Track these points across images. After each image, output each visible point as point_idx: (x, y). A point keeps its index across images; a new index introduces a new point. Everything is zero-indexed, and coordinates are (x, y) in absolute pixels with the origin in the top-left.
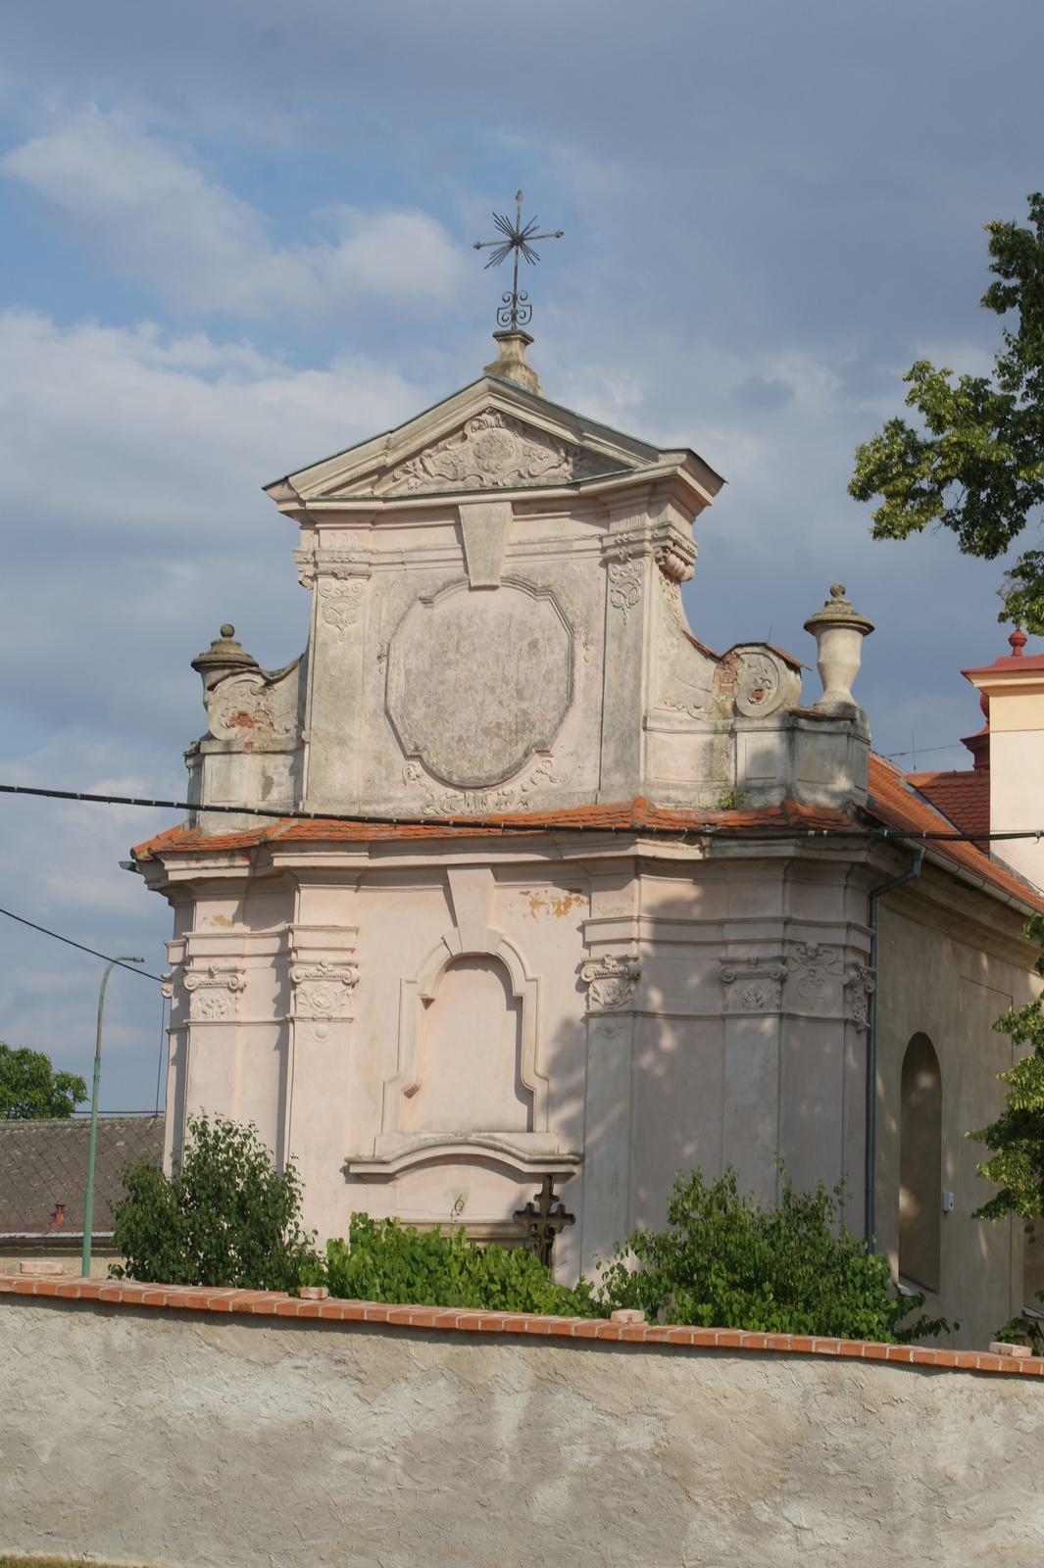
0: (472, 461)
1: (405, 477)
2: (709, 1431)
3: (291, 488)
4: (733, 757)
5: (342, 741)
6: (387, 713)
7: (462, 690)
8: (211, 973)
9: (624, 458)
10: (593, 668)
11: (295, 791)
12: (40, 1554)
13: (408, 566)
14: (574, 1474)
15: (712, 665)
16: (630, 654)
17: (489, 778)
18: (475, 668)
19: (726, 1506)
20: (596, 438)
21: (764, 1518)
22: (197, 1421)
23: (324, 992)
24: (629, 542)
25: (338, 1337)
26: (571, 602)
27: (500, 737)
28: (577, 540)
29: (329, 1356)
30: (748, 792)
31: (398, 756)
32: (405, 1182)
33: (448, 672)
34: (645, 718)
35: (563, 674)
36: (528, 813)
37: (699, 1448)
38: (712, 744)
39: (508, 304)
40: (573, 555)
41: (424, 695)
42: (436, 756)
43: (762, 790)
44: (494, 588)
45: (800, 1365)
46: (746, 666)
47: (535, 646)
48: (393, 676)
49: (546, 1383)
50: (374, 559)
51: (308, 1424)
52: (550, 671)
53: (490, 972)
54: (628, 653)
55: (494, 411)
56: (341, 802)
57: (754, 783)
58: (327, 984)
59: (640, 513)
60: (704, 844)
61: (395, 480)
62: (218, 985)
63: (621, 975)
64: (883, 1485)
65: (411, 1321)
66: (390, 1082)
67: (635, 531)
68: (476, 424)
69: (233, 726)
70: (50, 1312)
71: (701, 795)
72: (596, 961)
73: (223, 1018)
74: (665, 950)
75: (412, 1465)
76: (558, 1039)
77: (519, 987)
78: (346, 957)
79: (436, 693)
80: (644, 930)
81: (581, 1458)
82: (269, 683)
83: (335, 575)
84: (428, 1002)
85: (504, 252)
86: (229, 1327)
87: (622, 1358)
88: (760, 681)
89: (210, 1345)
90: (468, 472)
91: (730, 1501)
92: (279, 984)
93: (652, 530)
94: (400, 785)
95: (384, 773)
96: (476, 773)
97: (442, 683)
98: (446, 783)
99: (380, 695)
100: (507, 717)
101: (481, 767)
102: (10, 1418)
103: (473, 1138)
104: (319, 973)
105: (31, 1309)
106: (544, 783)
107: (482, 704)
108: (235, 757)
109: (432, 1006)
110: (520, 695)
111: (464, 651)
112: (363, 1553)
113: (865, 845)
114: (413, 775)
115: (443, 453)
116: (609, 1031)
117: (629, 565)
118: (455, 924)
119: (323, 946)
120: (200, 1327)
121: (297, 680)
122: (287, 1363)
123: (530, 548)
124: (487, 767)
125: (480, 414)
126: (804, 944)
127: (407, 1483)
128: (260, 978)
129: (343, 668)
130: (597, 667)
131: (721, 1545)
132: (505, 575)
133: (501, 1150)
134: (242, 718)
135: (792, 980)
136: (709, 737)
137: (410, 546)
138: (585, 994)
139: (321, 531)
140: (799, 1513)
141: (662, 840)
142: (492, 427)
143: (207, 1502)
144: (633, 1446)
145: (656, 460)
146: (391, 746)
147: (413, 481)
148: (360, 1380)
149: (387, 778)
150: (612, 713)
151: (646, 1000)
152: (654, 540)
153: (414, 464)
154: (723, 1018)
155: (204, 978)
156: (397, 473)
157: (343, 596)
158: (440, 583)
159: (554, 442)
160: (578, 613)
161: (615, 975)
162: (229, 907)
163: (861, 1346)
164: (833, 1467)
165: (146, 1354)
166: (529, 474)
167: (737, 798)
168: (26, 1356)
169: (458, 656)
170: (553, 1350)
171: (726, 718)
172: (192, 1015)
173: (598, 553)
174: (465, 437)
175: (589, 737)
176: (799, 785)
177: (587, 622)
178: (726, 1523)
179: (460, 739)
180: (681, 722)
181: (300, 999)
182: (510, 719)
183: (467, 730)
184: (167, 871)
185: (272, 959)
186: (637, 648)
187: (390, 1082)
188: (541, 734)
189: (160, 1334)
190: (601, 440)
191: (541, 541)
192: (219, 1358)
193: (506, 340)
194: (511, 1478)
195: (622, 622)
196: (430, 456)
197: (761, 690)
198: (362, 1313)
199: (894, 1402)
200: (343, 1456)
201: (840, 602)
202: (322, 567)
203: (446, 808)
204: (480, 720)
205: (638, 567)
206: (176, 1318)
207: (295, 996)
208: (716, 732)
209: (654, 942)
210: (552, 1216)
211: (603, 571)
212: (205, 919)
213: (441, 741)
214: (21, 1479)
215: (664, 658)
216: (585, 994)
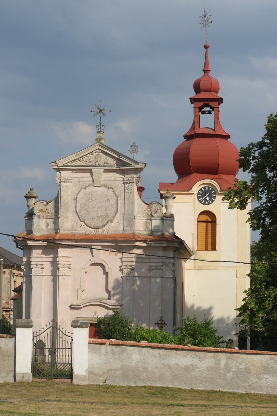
1: (79, 161)
2: (253, 365)
3: (56, 163)
4: (151, 224)
5: (67, 217)
6: (76, 211)
7: (93, 208)
8: (37, 265)
9: (130, 163)
10: (122, 205)
11: (54, 227)
12: (150, 385)
13: (80, 181)
14: (233, 372)
15: (146, 206)
16: (131, 203)
17: (99, 227)
18: (96, 203)
19: (256, 376)
20: (123, 158)
21: (261, 377)
22: (174, 365)
23: (64, 270)
24: (130, 180)
25: (197, 352)
26: (116, 191)
27: (101, 218)
28: (118, 178)
29: (195, 355)
30: (155, 232)
31: (79, 221)
32: (83, 309)
33: (89, 204)
34: (135, 217)
35: (115, 206)
36: (108, 234)
37: (251, 368)
39: (99, 125)
40: (117, 181)
41: (84, 208)
42: (87, 221)
43: (158, 232)
44: (99, 187)
45: (266, 356)
46: (153, 206)
47: (109, 200)
48: (77, 204)
49: (228, 359)
50: (72, 179)
52: (112, 205)
54: (130, 203)
55: (99, 149)
56: (67, 230)
57: (156, 230)
58: (65, 268)
59: (133, 174)
60: (147, 243)
61: (76, 162)
62: (38, 267)
63: (130, 269)
65: (209, 350)
66: (79, 289)
68: (95, 152)
69: (40, 212)
70: (150, 349)
71: (145, 232)
72: (124, 266)
73: (40, 275)
75: (208, 370)
76: (114, 282)
77: (107, 270)
78: (69, 263)
79: (87, 208)
80: (134, 260)
82: (47, 203)
83: (65, 182)
84: (86, 272)
85: (98, 113)
86: (179, 351)
87: (240, 355)
88: (156, 209)
89: (176, 354)
90: (93, 161)
91: (256, 375)
92: (52, 268)
93: (136, 178)
94: (79, 227)
95: (76, 225)
96: (96, 226)
97: (88, 206)
99: (74, 208)
101: (97, 224)
103: (98, 300)
104: (64, 266)
105: (147, 348)
106: (111, 228)
107: (97, 211)
108: (40, 219)
109: (87, 273)
110: (106, 210)
111: (93, 200)
112: (201, 383)
113: (178, 243)
114: (82, 225)
115: (88, 157)
117: (130, 184)
119: (64, 260)
120: (174, 351)
121: (54, 203)
122: (188, 356)
123: (107, 179)
124: (99, 224)
125: (96, 150)
126: (165, 262)
127: (207, 373)
128: (48, 268)
129: (67, 202)
130: (122, 205)
131: (255, 381)
132: (102, 184)
133: (105, 303)
134: (41, 210)
136: (146, 220)
137: (80, 176)
138: (121, 272)
139: (61, 173)
140: (266, 376)
141: (140, 242)
142: (98, 152)
144: (242, 367)
145: (138, 164)
146: (77, 219)
147: (80, 162)
148: (200, 359)
150: (126, 215)
152: (136, 180)
153: (81, 159)
155: (35, 266)
156: (77, 160)
158: (87, 185)
159: (112, 157)
160: (118, 193)
161: (129, 269)
162: (40, 251)
164: (271, 370)
165: (166, 355)
166: (106, 163)
167: (152, 233)
168: (146, 355)
169: (92, 201)
171: (149, 217)
172: (32, 274)
173: (122, 181)
174: (92, 154)
175: (121, 219)
176: (164, 231)
177: (120, 195)
178: (256, 378)
179: (93, 218)
180: (140, 217)
182: (104, 215)
183: (94, 216)
184: (28, 243)
185: (50, 262)
186: (132, 202)
187: (79, 289)
188: (111, 218)
190: (124, 158)
191: (110, 177)
192: (177, 355)
193: (100, 133)
194: (223, 372)
195: (128, 196)
196: (84, 157)
197: (157, 211)
198: (226, 350)
200: (197, 370)
201: (170, 193)
202: (62, 180)
204: (97, 214)
205: (132, 185)
206: (171, 350)
207: (59, 271)
208: (147, 219)
209: (136, 262)
210: (163, 324)
212: (35, 253)
213: (88, 218)
214: (146, 374)
216: (121, 272)
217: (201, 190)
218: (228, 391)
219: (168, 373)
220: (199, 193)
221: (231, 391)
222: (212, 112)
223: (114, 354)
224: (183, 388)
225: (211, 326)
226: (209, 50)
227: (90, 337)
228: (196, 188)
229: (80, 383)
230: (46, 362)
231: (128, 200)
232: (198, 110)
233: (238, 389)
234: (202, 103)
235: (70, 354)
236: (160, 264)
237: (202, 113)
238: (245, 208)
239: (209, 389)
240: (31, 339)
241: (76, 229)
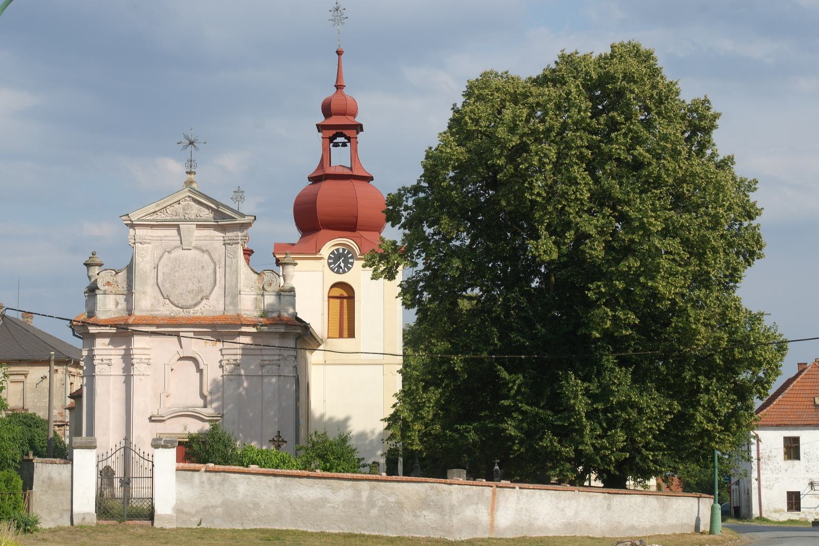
0: (181, 211)
1: (160, 214)
3: (129, 217)
8: (102, 360)
9: (233, 216)
12: (263, 527)
15: (256, 276)
18: (185, 273)
19: (411, 512)
29: (326, 484)
32: (167, 422)
34: (240, 291)
35: (212, 276)
36: (203, 316)
38: (256, 298)
43: (272, 312)
44: (190, 249)
45: (425, 484)
49: (372, 489)
53: (191, 362)
55: (189, 197)
56: (144, 311)
59: (237, 231)
61: (157, 214)
64: (442, 507)
67: (236, 236)
68: (183, 200)
74: (245, 357)
77: (202, 367)
78: (148, 357)
81: (380, 504)
82: (117, 273)
83: (141, 243)
85: (187, 146)
87: (388, 483)
92: (124, 364)
95: (157, 303)
97: (175, 277)
98: (176, 306)
102: (254, 499)
103: (190, 409)
107: (187, 284)
110: (199, 281)
112: (335, 524)
114: (166, 303)
115: (173, 208)
116: (231, 380)
118: (181, 347)
120: (297, 479)
124: (189, 302)
127: (343, 510)
133: (199, 413)
134: (108, 283)
135: (281, 365)
136: (255, 296)
140: (425, 513)
143: (299, 515)
145: (245, 218)
147: (163, 215)
149: (158, 304)
151: (240, 372)
154: (262, 376)
155: (100, 361)
156: (158, 213)
159: (208, 207)
161: (233, 364)
164: (432, 503)
165: (285, 485)
167: (265, 314)
170: (374, 482)
174: (179, 203)
179: (181, 294)
181: (134, 369)
185: (121, 356)
186: (237, 271)
191: (205, 236)
192: (301, 485)
194: (365, 508)
199: (444, 491)
200: (329, 505)
203: (177, 314)
208: (258, 295)
211: (224, 247)
215: (244, 273)
217: (333, 253)
218: (373, 534)
220: (330, 258)
221: (377, 533)
222: (348, 144)
224: (309, 530)
226: (343, 57)
227: (178, 461)
228: (327, 250)
229: (164, 527)
230: (116, 497)
232: (328, 140)
234: (334, 132)
235: (150, 485)
236: (277, 358)
237: (333, 146)
238: (395, 278)
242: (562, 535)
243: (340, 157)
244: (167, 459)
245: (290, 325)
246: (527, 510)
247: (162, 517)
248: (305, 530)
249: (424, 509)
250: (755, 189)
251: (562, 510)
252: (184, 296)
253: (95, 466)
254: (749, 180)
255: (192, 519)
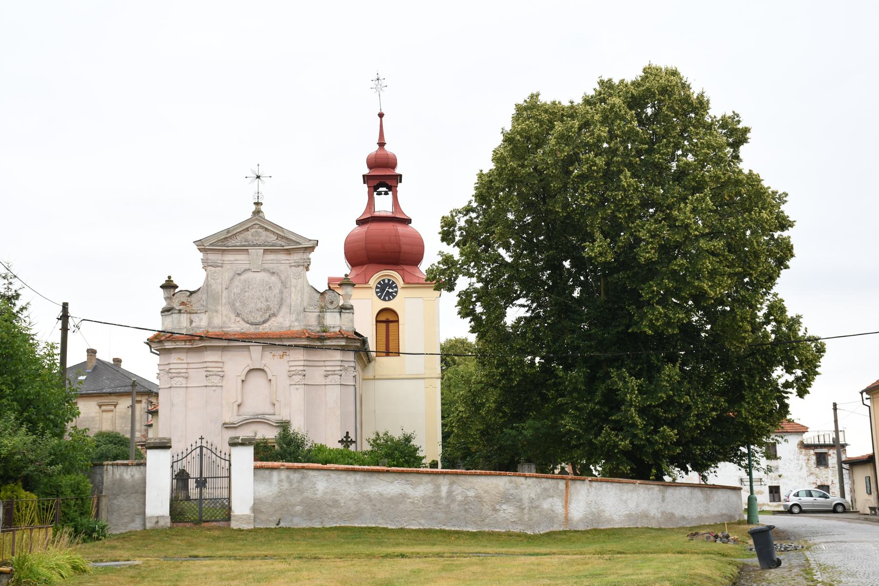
2: (486, 492)
5: (217, 311)
12: (342, 525)
49: (452, 484)
51: (401, 494)
75: (424, 501)
78: (220, 369)
97: (244, 296)
100: (263, 306)
103: (259, 416)
106: (275, 324)
110: (267, 301)
122: (396, 482)
127: (423, 505)
133: (268, 420)
134: (183, 303)
136: (318, 313)
140: (504, 507)
143: (379, 512)
154: (325, 385)
157: (215, 272)
158: (243, 270)
159: (274, 233)
163: (442, 468)
165: (364, 481)
174: (248, 230)
189: (368, 478)
191: (272, 260)
199: (522, 484)
200: (409, 500)
217: (379, 283)
218: (453, 529)
219: (369, 507)
220: (377, 287)
221: (457, 529)
222: (390, 193)
223: (290, 482)
224: (390, 527)
225: (411, 443)
226: (383, 118)
227: (255, 460)
228: (373, 281)
229: (242, 528)
230: (192, 498)
231: (296, 288)
232: (372, 189)
233: (466, 526)
234: (378, 182)
235: (227, 485)
236: (339, 368)
237: (377, 194)
238: (454, 289)
239: (425, 527)
240: (170, 466)
241: (229, 325)
242: (627, 527)
243: (383, 204)
244: (244, 458)
245: (351, 339)
246: (596, 503)
247: (241, 518)
248: (385, 526)
249: (504, 503)
250: (786, 201)
251: (625, 502)
252: (253, 314)
253: (170, 466)
254: (779, 193)
255: (270, 519)
